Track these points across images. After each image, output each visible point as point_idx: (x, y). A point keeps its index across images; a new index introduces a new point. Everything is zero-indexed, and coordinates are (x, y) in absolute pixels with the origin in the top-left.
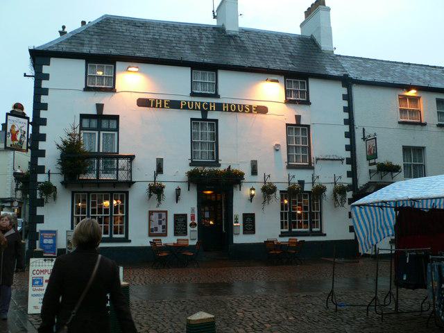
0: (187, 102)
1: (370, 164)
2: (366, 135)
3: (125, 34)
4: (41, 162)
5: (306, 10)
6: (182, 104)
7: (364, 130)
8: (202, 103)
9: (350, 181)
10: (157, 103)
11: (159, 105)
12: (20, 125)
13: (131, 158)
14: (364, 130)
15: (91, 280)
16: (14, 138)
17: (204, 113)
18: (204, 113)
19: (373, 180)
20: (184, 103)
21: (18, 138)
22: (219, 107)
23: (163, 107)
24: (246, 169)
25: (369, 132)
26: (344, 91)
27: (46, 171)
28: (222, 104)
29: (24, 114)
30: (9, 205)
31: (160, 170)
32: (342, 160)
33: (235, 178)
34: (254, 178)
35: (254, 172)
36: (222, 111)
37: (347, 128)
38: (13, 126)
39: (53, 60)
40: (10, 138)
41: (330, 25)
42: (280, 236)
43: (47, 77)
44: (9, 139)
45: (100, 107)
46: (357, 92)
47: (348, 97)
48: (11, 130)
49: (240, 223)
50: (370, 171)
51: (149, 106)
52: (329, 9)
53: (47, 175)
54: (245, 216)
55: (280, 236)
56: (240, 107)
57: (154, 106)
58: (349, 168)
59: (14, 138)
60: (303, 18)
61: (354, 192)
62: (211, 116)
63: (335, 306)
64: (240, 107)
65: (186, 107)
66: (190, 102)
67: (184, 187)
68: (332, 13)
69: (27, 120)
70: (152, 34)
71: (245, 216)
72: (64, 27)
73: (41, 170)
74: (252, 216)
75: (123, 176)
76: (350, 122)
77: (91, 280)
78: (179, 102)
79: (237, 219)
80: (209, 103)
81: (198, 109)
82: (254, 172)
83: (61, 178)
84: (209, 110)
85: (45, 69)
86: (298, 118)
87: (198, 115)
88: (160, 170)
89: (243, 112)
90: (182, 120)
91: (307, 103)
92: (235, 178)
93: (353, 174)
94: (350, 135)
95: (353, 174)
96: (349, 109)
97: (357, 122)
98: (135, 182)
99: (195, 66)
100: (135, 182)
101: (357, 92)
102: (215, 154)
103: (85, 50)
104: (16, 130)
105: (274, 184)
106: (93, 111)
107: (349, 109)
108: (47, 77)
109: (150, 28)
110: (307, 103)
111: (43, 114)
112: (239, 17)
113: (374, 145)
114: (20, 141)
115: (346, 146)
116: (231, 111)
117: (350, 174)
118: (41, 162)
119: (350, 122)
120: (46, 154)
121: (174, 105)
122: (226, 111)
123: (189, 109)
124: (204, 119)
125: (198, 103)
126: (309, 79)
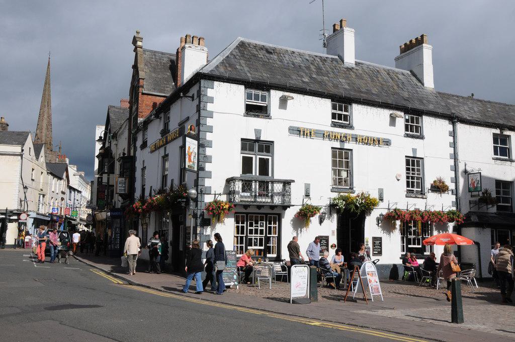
8: (341, 133)
13: (287, 183)
15: (494, 291)
19: (472, 210)
21: (192, 160)
22: (356, 139)
24: (374, 195)
27: (213, 192)
30: (15, 217)
33: (368, 206)
39: (216, 83)
46: (460, 127)
47: (453, 134)
54: (375, 239)
60: (398, 53)
62: (347, 146)
71: (375, 239)
72: (473, 95)
74: (380, 239)
75: (277, 200)
76: (455, 157)
77: (494, 291)
79: (367, 242)
82: (381, 200)
83: (385, 212)
86: (258, 132)
87: (337, 145)
90: (325, 148)
91: (421, 137)
92: (368, 206)
94: (455, 168)
96: (454, 145)
99: (248, 85)
104: (191, 151)
107: (454, 145)
110: (421, 137)
115: (451, 178)
119: (455, 157)
126: (424, 117)
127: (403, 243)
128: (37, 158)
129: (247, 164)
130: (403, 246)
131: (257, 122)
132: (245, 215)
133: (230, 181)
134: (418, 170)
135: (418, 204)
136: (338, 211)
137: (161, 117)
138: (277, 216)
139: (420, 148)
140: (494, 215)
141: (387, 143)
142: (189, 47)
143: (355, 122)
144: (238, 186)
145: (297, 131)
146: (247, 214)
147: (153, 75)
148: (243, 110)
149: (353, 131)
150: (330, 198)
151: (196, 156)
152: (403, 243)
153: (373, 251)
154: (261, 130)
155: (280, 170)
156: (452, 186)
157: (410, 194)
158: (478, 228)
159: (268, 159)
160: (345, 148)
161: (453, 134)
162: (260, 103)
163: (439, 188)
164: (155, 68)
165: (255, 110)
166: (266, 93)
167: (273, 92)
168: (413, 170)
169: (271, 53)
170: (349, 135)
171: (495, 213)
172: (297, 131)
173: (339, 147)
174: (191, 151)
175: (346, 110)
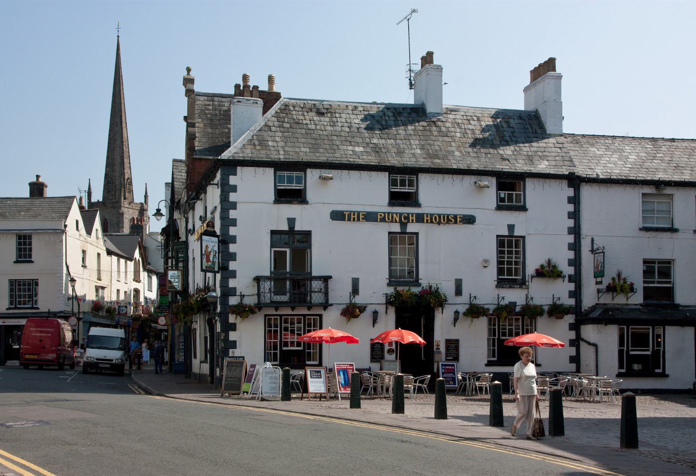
0: (384, 213)
1: (597, 283)
2: (595, 247)
3: (310, 126)
4: (232, 283)
5: (533, 69)
6: (379, 217)
7: (593, 240)
8: (401, 214)
9: (572, 302)
10: (352, 216)
11: (354, 218)
12: (212, 244)
13: (326, 279)
14: (593, 240)
16: (208, 260)
17: (403, 225)
18: (403, 225)
19: (602, 301)
20: (381, 215)
21: (211, 260)
22: (420, 218)
23: (358, 220)
24: (447, 289)
25: (598, 243)
26: (571, 192)
27: (238, 293)
28: (423, 214)
29: (215, 232)
31: (355, 291)
32: (99, 279)
34: (459, 299)
35: (459, 292)
36: (423, 222)
37: (571, 239)
38: (207, 247)
39: (239, 169)
40: (205, 259)
41: (560, 98)
42: (486, 365)
43: (234, 189)
44: (204, 260)
45: (291, 222)
46: (587, 192)
47: (575, 200)
48: (205, 251)
49: (443, 349)
50: (599, 291)
51: (343, 219)
52: (560, 77)
53: (239, 297)
54: (448, 342)
55: (486, 365)
56: (444, 217)
57: (349, 220)
58: (572, 286)
59: (208, 260)
60: (527, 81)
61: (576, 316)
62: (411, 228)
63: (296, 109)
64: (444, 217)
65: (383, 220)
66: (389, 213)
67: (381, 309)
68: (564, 82)
69: (217, 239)
70: (340, 124)
71: (448, 342)
73: (233, 292)
76: (576, 231)
78: (376, 213)
79: (438, 345)
80: (408, 214)
81: (396, 222)
82: (459, 292)
84: (409, 221)
85: (233, 180)
86: (511, 228)
87: (396, 228)
88: (355, 291)
89: (448, 223)
90: (380, 233)
93: (576, 294)
94: (575, 247)
95: (576, 294)
96: (575, 215)
97: (585, 230)
98: (332, 305)
100: (332, 305)
101: (587, 192)
102: (275, 174)
103: (274, 157)
104: (209, 250)
105: (486, 307)
106: (285, 227)
107: (575, 215)
108: (234, 189)
109: (337, 115)
110: (523, 208)
111: (232, 231)
112: (444, 86)
113: (602, 261)
114: (213, 261)
116: (433, 223)
117: (572, 294)
118: (232, 283)
119: (576, 231)
120: (238, 274)
121: (370, 217)
122: (427, 222)
123: (386, 222)
124: (403, 233)
125: (396, 214)
127: (494, 346)
128: (89, 231)
129: (278, 259)
130: (494, 350)
131: (291, 210)
132: (302, 317)
133: (258, 279)
134: (517, 253)
135: (515, 296)
136: (190, 296)
137: (202, 199)
138: (318, 317)
139: (521, 223)
140: (639, 307)
141: (469, 220)
142: (238, 102)
143: (422, 198)
144: (267, 286)
145: (337, 216)
146: (281, 316)
147: (209, 130)
148: (272, 196)
149: (420, 209)
150: (386, 294)
151: (217, 255)
152: (494, 346)
153: (447, 355)
154: (295, 219)
155: (319, 264)
156: (569, 271)
157: (501, 283)
158: (596, 325)
159: (286, 251)
160: (408, 231)
161: (575, 200)
162: (294, 186)
163: (548, 272)
164: (211, 120)
165: (284, 196)
166: (302, 174)
167: (309, 171)
168: (510, 252)
169: (322, 114)
170: (412, 214)
171: (640, 305)
172: (337, 216)
173: (399, 231)
174: (209, 250)
175: (411, 184)
